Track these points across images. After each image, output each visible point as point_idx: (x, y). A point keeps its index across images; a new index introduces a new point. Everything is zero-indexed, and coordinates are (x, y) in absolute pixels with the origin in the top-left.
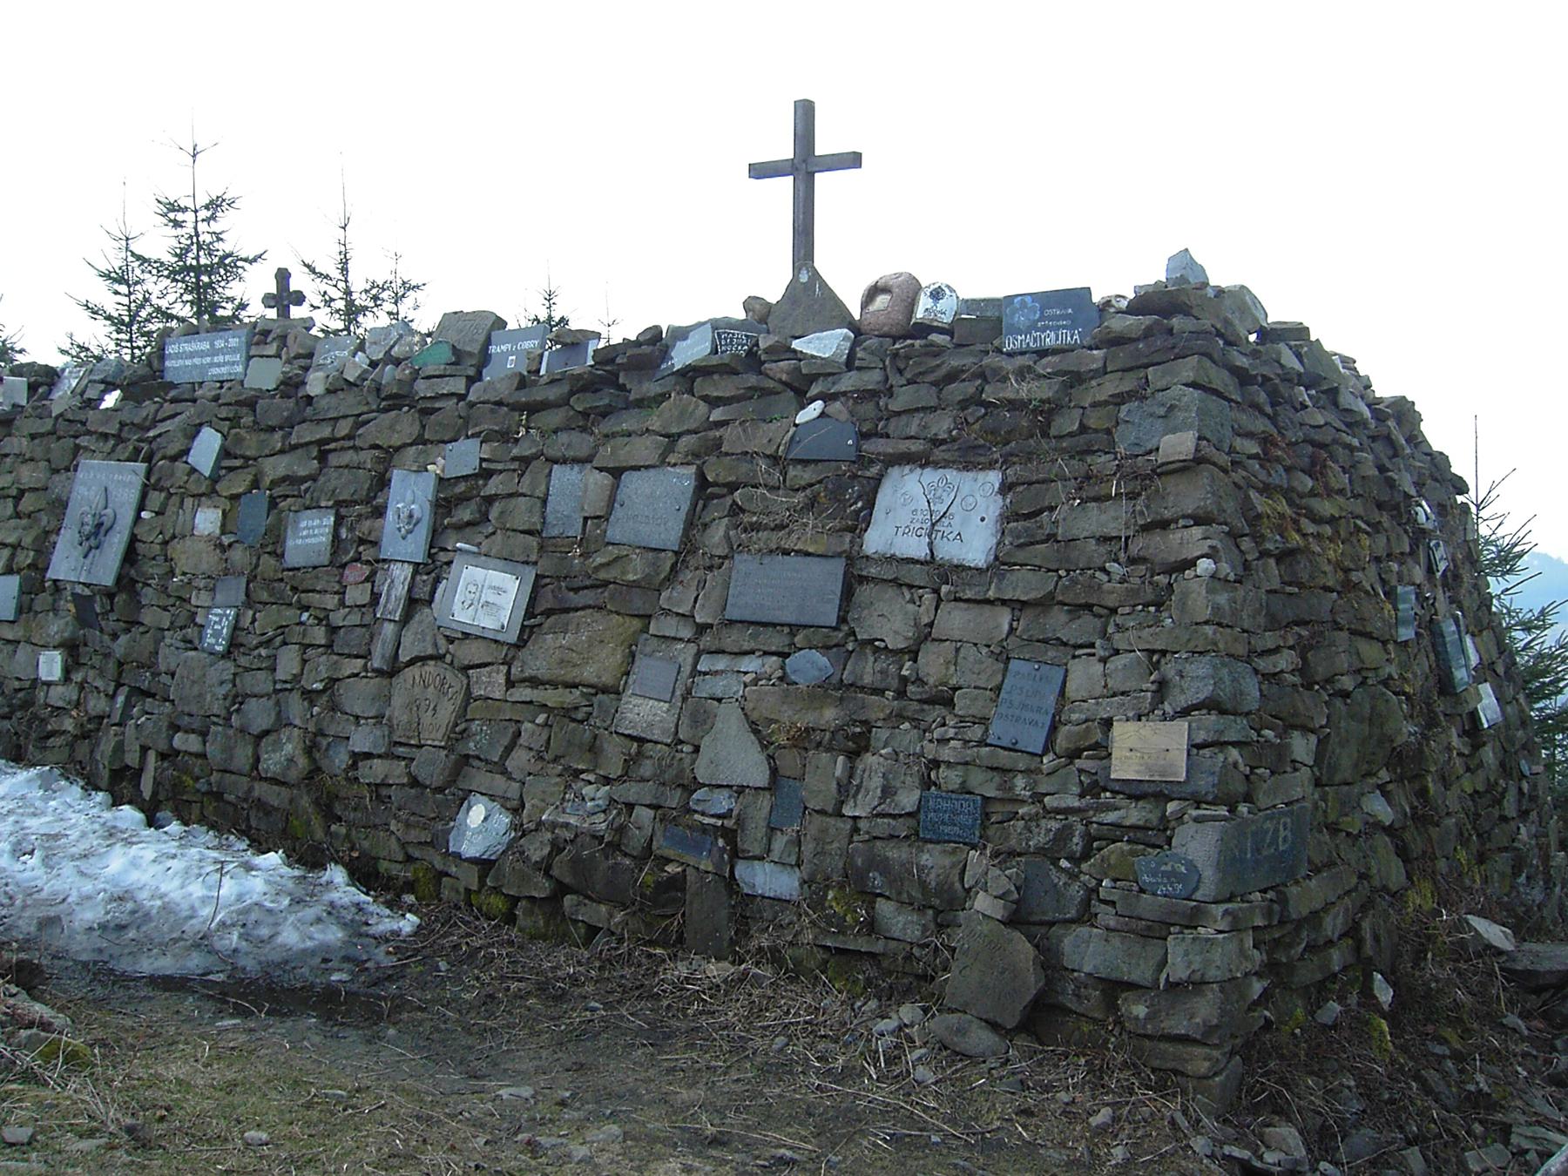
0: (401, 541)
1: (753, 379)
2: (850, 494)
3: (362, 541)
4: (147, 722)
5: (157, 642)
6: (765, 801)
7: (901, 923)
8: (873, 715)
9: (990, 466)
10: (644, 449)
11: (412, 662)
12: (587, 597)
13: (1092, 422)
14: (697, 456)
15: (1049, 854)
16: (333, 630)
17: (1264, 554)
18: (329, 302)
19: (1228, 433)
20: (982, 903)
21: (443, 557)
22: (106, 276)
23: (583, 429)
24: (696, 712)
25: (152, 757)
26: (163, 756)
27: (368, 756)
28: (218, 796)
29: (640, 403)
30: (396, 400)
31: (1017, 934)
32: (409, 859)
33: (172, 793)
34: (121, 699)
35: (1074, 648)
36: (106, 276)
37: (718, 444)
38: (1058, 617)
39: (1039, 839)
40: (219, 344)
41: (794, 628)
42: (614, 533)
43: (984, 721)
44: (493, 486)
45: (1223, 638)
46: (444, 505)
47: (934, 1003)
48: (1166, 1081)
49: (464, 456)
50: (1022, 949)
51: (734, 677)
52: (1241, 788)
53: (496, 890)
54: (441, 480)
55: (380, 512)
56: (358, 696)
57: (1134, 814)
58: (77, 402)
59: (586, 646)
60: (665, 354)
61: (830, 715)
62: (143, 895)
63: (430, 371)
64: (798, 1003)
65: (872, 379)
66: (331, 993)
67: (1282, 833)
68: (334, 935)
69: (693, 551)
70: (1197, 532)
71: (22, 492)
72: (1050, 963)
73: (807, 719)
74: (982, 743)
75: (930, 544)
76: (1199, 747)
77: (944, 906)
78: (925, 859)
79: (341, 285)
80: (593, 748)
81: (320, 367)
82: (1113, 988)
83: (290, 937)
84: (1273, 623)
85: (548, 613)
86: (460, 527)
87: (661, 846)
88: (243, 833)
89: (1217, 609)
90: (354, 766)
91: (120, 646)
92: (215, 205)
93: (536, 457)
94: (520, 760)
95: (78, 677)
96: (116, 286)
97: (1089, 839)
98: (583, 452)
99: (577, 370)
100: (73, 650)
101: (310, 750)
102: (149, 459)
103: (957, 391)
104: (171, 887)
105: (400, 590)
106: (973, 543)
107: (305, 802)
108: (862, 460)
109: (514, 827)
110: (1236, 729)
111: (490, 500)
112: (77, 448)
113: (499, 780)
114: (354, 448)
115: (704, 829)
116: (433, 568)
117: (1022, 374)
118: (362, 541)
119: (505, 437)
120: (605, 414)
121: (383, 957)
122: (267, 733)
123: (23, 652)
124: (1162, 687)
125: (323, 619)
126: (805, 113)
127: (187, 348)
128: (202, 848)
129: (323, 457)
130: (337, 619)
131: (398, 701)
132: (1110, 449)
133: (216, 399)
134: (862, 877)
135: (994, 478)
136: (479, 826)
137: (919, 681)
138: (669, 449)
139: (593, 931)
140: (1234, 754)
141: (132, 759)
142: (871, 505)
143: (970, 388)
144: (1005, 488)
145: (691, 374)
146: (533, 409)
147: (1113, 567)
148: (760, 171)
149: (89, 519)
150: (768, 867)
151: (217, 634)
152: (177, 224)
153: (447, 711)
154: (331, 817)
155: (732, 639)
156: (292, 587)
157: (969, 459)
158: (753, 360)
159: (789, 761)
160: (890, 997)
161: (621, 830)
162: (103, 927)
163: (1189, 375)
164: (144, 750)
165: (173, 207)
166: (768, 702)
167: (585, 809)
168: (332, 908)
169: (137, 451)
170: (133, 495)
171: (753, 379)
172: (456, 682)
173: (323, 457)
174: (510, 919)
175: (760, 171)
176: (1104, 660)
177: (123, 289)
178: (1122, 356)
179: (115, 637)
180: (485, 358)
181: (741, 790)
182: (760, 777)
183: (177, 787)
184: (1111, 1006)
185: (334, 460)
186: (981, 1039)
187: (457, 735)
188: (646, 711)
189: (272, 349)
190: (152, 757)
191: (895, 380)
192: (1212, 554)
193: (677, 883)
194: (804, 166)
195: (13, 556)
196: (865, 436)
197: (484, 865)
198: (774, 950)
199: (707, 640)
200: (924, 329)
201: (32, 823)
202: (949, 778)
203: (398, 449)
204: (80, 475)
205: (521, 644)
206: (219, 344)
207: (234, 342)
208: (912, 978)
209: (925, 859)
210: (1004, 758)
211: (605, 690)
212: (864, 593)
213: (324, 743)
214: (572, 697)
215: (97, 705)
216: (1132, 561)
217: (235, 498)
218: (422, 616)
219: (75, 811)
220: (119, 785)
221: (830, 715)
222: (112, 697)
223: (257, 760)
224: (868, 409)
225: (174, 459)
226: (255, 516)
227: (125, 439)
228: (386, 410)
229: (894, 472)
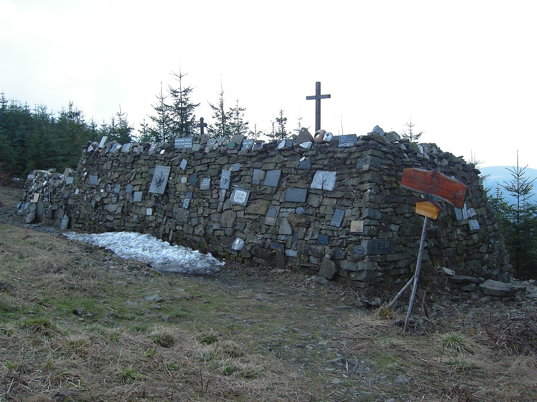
0: (224, 185)
1: (292, 152)
2: (309, 176)
3: (216, 185)
4: (171, 223)
5: (173, 206)
6: (291, 237)
7: (314, 260)
8: (311, 220)
9: (334, 171)
10: (271, 166)
11: (225, 210)
12: (260, 196)
13: (353, 162)
14: (281, 168)
15: (340, 247)
16: (210, 203)
17: (385, 189)
18: (218, 116)
19: (379, 164)
20: (327, 256)
21: (232, 188)
22: (157, 109)
23: (260, 162)
24: (279, 219)
25: (172, 231)
26: (174, 231)
27: (217, 230)
28: (186, 239)
29: (271, 156)
30: (224, 154)
31: (332, 262)
32: (224, 251)
33: (177, 239)
34: (165, 219)
35: (347, 207)
36: (157, 109)
37: (285, 165)
38: (345, 200)
39: (338, 244)
40: (186, 140)
41: (298, 203)
42: (265, 183)
43: (330, 221)
44: (242, 173)
45: (372, 205)
46: (232, 177)
47: (318, 276)
48: (357, 289)
49: (236, 167)
50: (333, 264)
51: (286, 213)
52: (375, 234)
53: (241, 257)
54: (232, 172)
55: (220, 178)
56: (214, 217)
57: (354, 239)
58: (155, 152)
59: (259, 207)
60: (277, 146)
61: (303, 220)
62: (170, 258)
63: (230, 148)
64: (294, 276)
65: (314, 152)
66: (206, 274)
67: (386, 244)
68: (208, 265)
69: (280, 187)
70: (368, 184)
71: (142, 173)
72: (338, 267)
73: (300, 221)
74: (329, 225)
75: (322, 187)
76: (366, 226)
77: (321, 257)
78: (318, 248)
79: (221, 111)
80: (260, 227)
81: (208, 146)
82: (349, 272)
83: (199, 265)
84: (387, 202)
85: (252, 200)
86: (236, 182)
87: (272, 247)
88: (190, 247)
89: (370, 199)
90: (214, 232)
91: (165, 207)
92: (186, 91)
93: (251, 167)
94: (246, 230)
95: (155, 214)
96: (159, 112)
97: (347, 244)
98: (260, 167)
99: (259, 149)
100: (154, 208)
101: (205, 229)
102: (171, 166)
103: (331, 155)
104: (176, 257)
105: (224, 195)
106: (330, 186)
107: (204, 240)
108: (311, 169)
109: (244, 244)
110: (374, 222)
111: (242, 176)
112: (155, 163)
113: (242, 234)
114: (215, 165)
115: (280, 243)
116: (230, 190)
117: (341, 152)
118: (216, 185)
119: (245, 163)
120: (264, 158)
121: (217, 269)
122: (196, 225)
123: (143, 209)
124: (361, 214)
125: (208, 201)
126: (318, 85)
127: (179, 141)
128: (182, 250)
129: (208, 166)
130: (211, 201)
131: (222, 218)
132: (355, 168)
133: (186, 152)
134: (308, 252)
135: (335, 173)
136: (238, 244)
137: (320, 213)
138: (276, 166)
139: (259, 264)
140: (372, 227)
141: (167, 232)
142: (313, 178)
143: (331, 155)
144: (337, 175)
145: (281, 150)
146: (251, 157)
147: (354, 191)
148: (308, 98)
149: (158, 179)
150: (291, 250)
151: (186, 204)
152: (176, 96)
153: (232, 220)
154: (209, 243)
155: (287, 205)
156: (202, 194)
157: (331, 169)
158: (293, 148)
159: (296, 229)
160: (310, 275)
161: (264, 243)
162: (162, 263)
163: (370, 153)
164: (170, 230)
165: (175, 92)
166: (292, 219)
167: (257, 239)
168: (208, 261)
169: (169, 164)
170: (168, 174)
171: (292, 152)
172: (234, 214)
173: (208, 166)
174: (243, 262)
175: (308, 98)
176: (352, 209)
177: (161, 112)
178: (359, 148)
179: (164, 205)
180: (242, 145)
181: (287, 235)
182: (290, 233)
183: (177, 238)
184: (348, 275)
185: (210, 167)
186: (325, 281)
187: (234, 225)
188: (270, 220)
189: (198, 142)
190: (172, 231)
191: (319, 153)
192: (371, 189)
193: (274, 254)
194: (318, 97)
195: (141, 187)
196: (312, 164)
197: (238, 251)
198: (291, 266)
199: (282, 205)
200: (324, 142)
201: (146, 245)
202: (323, 232)
203: (224, 165)
204: (156, 169)
205: (247, 206)
206: (186, 140)
207: (190, 140)
208: (316, 272)
209: (318, 248)
210: (333, 228)
211: (263, 216)
212: (310, 195)
213: (208, 227)
214: (257, 217)
215: (159, 220)
216: (358, 190)
217: (190, 175)
218: (228, 200)
219: (155, 243)
220: (164, 237)
221: (303, 220)
222: (163, 218)
223: (194, 231)
224: (313, 159)
225: (177, 166)
226: (194, 179)
227: (165, 161)
228: (221, 156)
229: (317, 171)
